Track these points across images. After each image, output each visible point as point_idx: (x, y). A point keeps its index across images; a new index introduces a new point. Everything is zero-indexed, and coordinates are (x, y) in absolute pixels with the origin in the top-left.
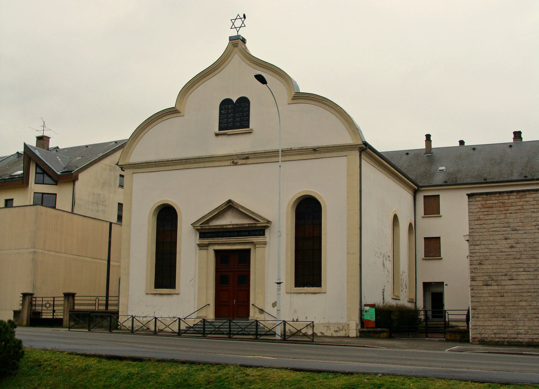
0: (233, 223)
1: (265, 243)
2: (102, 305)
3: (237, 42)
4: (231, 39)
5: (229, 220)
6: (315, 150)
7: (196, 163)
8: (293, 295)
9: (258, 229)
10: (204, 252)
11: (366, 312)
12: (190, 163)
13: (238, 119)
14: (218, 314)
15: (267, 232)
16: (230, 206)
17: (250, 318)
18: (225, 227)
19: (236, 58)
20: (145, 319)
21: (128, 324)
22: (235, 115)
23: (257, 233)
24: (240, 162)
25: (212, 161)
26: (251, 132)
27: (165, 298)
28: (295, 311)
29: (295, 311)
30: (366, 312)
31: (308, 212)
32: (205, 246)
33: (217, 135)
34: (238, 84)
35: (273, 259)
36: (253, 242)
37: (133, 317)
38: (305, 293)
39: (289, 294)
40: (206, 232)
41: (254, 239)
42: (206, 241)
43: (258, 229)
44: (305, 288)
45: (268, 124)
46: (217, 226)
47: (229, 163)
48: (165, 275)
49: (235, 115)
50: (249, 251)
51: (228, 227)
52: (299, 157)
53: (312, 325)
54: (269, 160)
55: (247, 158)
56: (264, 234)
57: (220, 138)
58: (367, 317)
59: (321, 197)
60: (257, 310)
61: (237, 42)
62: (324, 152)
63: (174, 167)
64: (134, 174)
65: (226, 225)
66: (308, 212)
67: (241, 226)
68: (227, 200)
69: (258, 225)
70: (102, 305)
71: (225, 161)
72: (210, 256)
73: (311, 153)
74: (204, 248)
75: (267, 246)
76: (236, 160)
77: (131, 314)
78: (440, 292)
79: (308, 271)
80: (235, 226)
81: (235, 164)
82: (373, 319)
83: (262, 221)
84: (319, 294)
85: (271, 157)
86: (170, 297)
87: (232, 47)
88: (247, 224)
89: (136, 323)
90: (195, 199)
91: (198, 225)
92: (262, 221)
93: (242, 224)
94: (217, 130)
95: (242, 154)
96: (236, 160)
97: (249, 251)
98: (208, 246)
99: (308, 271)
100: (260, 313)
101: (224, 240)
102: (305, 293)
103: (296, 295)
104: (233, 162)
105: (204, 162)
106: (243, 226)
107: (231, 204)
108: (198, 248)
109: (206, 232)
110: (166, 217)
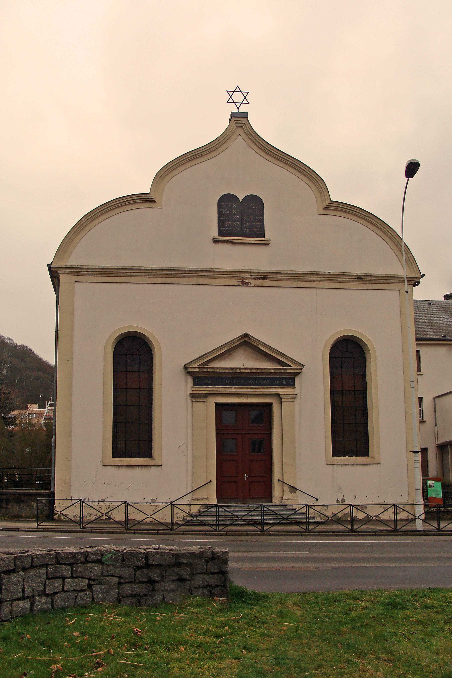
0: (246, 366)
1: (294, 396)
2: (19, 592)
3: (239, 120)
4: (234, 115)
5: (241, 362)
6: (360, 278)
7: (184, 277)
8: (335, 466)
9: (285, 375)
10: (199, 406)
11: (430, 487)
12: (175, 276)
13: (248, 224)
14: (221, 495)
15: (297, 380)
16: (246, 342)
17: (274, 500)
18: (238, 371)
19: (240, 141)
20: (101, 504)
21: (74, 513)
22: (241, 219)
23: (284, 382)
24: (253, 282)
25: (210, 277)
26: (268, 244)
27: (137, 471)
28: (340, 488)
29: (340, 488)
30: (430, 487)
31: (349, 356)
32: (203, 397)
33: (216, 241)
34: (245, 179)
35: (304, 420)
36: (279, 395)
37: (82, 502)
38: (353, 464)
39: (331, 466)
40: (202, 377)
41: (279, 390)
42: (204, 390)
43: (285, 375)
44: (347, 457)
45: (291, 239)
46: (226, 369)
47: (236, 282)
48: (133, 434)
49: (241, 219)
50: (269, 406)
51: (243, 371)
52: (337, 285)
53: (362, 508)
54: (295, 284)
55: (264, 278)
56: (293, 384)
57: (220, 245)
58: (431, 494)
59: (365, 336)
60: (286, 488)
61: (239, 120)
62: (370, 282)
63: (148, 280)
64: (77, 284)
65: (240, 369)
66: (349, 356)
67: (263, 371)
68: (243, 333)
69: (288, 371)
70: (19, 592)
71: (231, 278)
72: (208, 410)
73: (353, 282)
74: (202, 400)
75: (297, 401)
76: (245, 279)
77: (76, 495)
78: (336, 458)
79: (351, 433)
80: (254, 371)
81: (247, 285)
82: (440, 496)
83: (294, 366)
84: (371, 466)
85: (299, 280)
86: (145, 470)
87: (235, 126)
88: (272, 369)
89: (87, 510)
90: (185, 331)
91: (195, 366)
92: (294, 366)
93: (265, 369)
94: (215, 234)
95: (259, 273)
96: (245, 279)
97: (269, 406)
98: (206, 397)
99: (351, 433)
100: (291, 493)
101: (233, 389)
102: (353, 464)
103: (340, 467)
104: (243, 282)
105: (197, 277)
106: (266, 371)
107: (247, 339)
108: (189, 400)
109: (202, 377)
110: (133, 355)
